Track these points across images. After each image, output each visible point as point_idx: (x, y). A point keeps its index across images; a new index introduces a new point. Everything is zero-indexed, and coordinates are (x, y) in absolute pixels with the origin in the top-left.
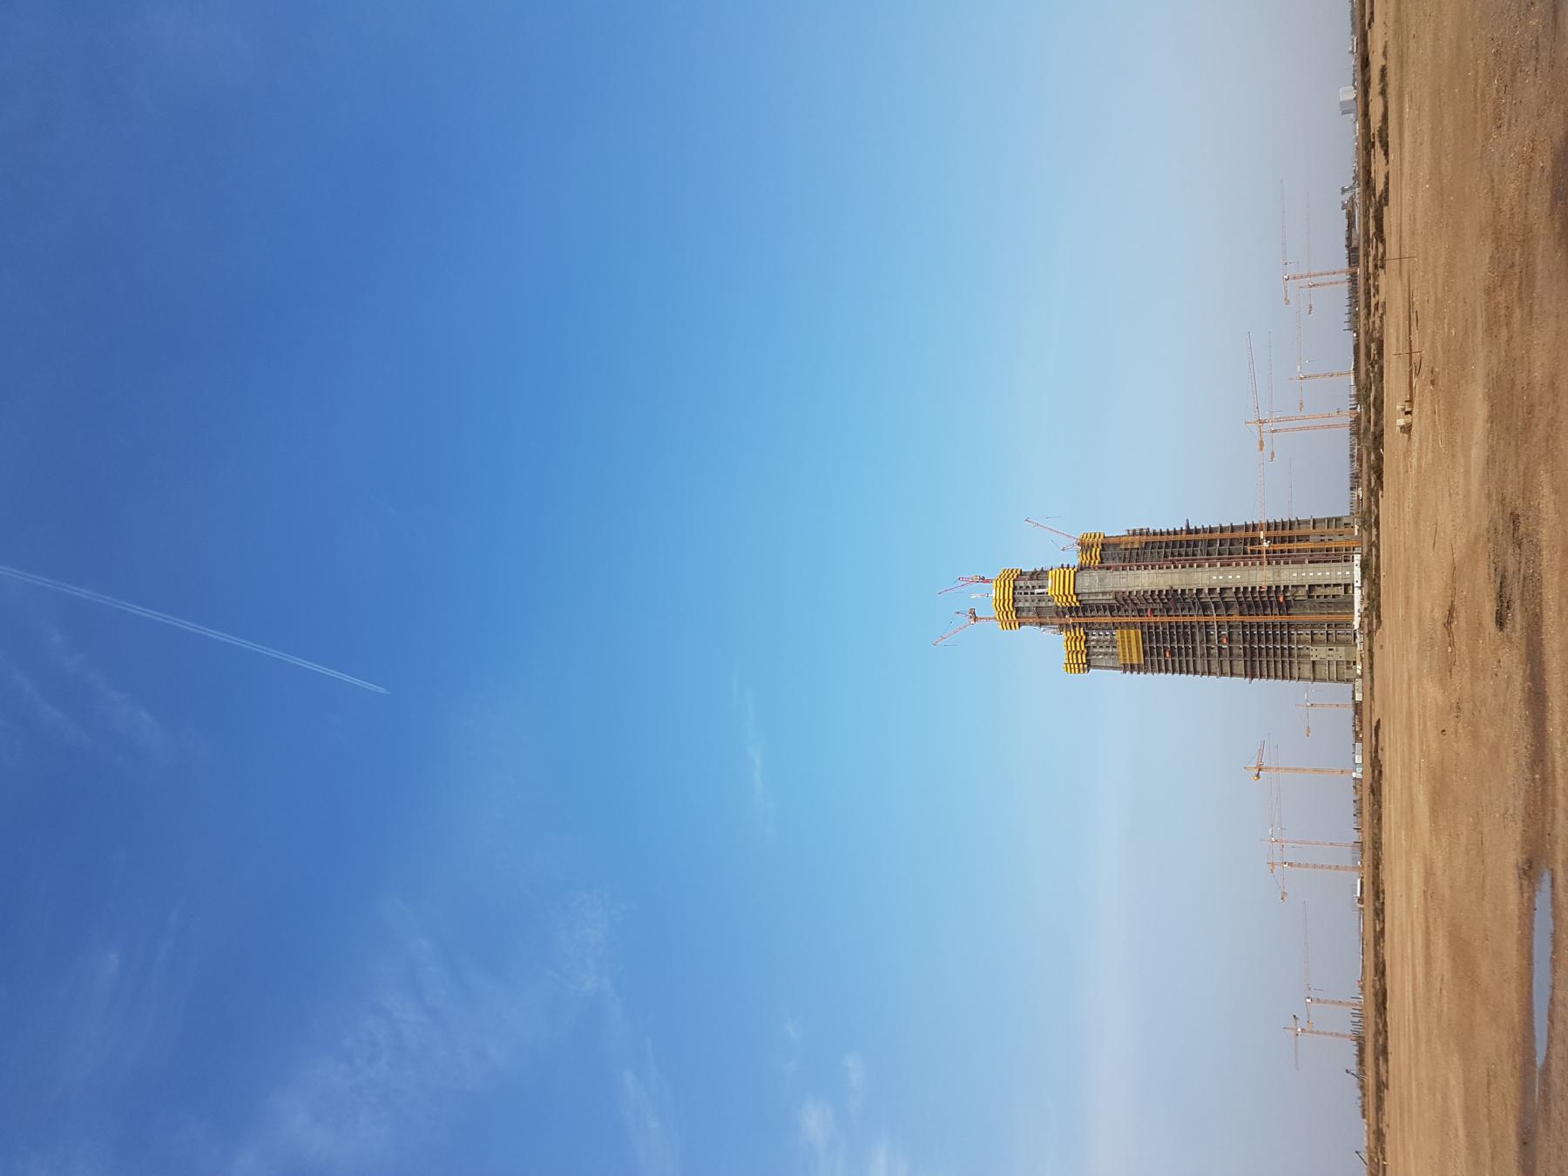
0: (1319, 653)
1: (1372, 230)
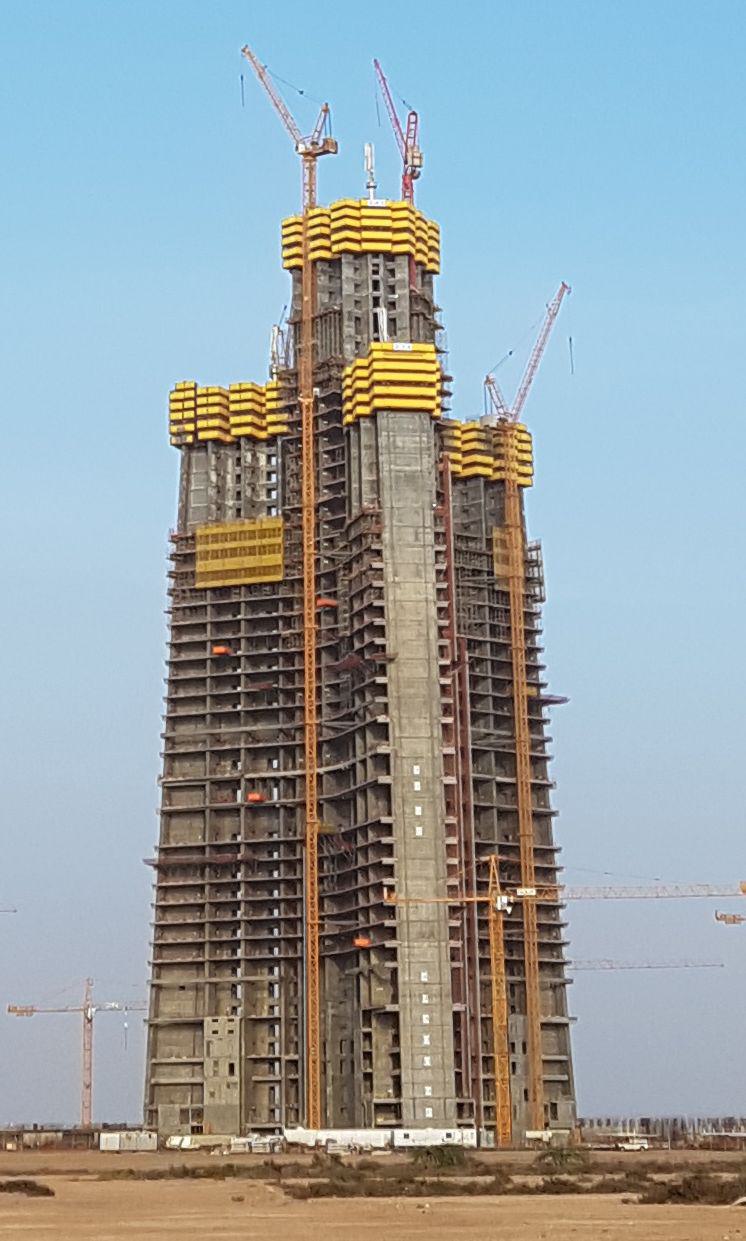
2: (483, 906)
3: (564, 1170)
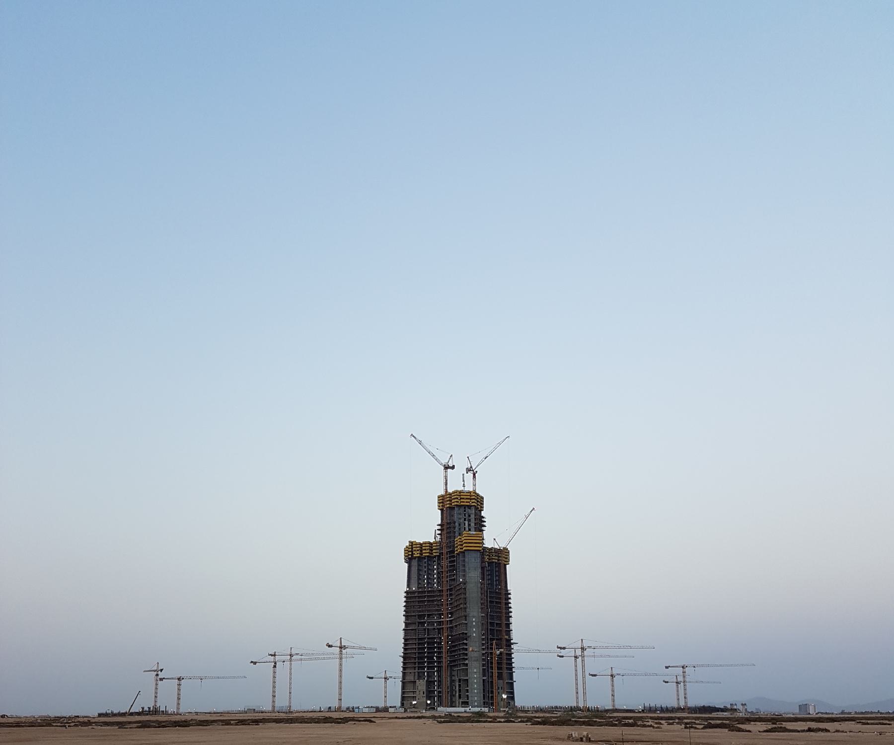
1: (712, 722)
2: (491, 653)
3: (514, 714)
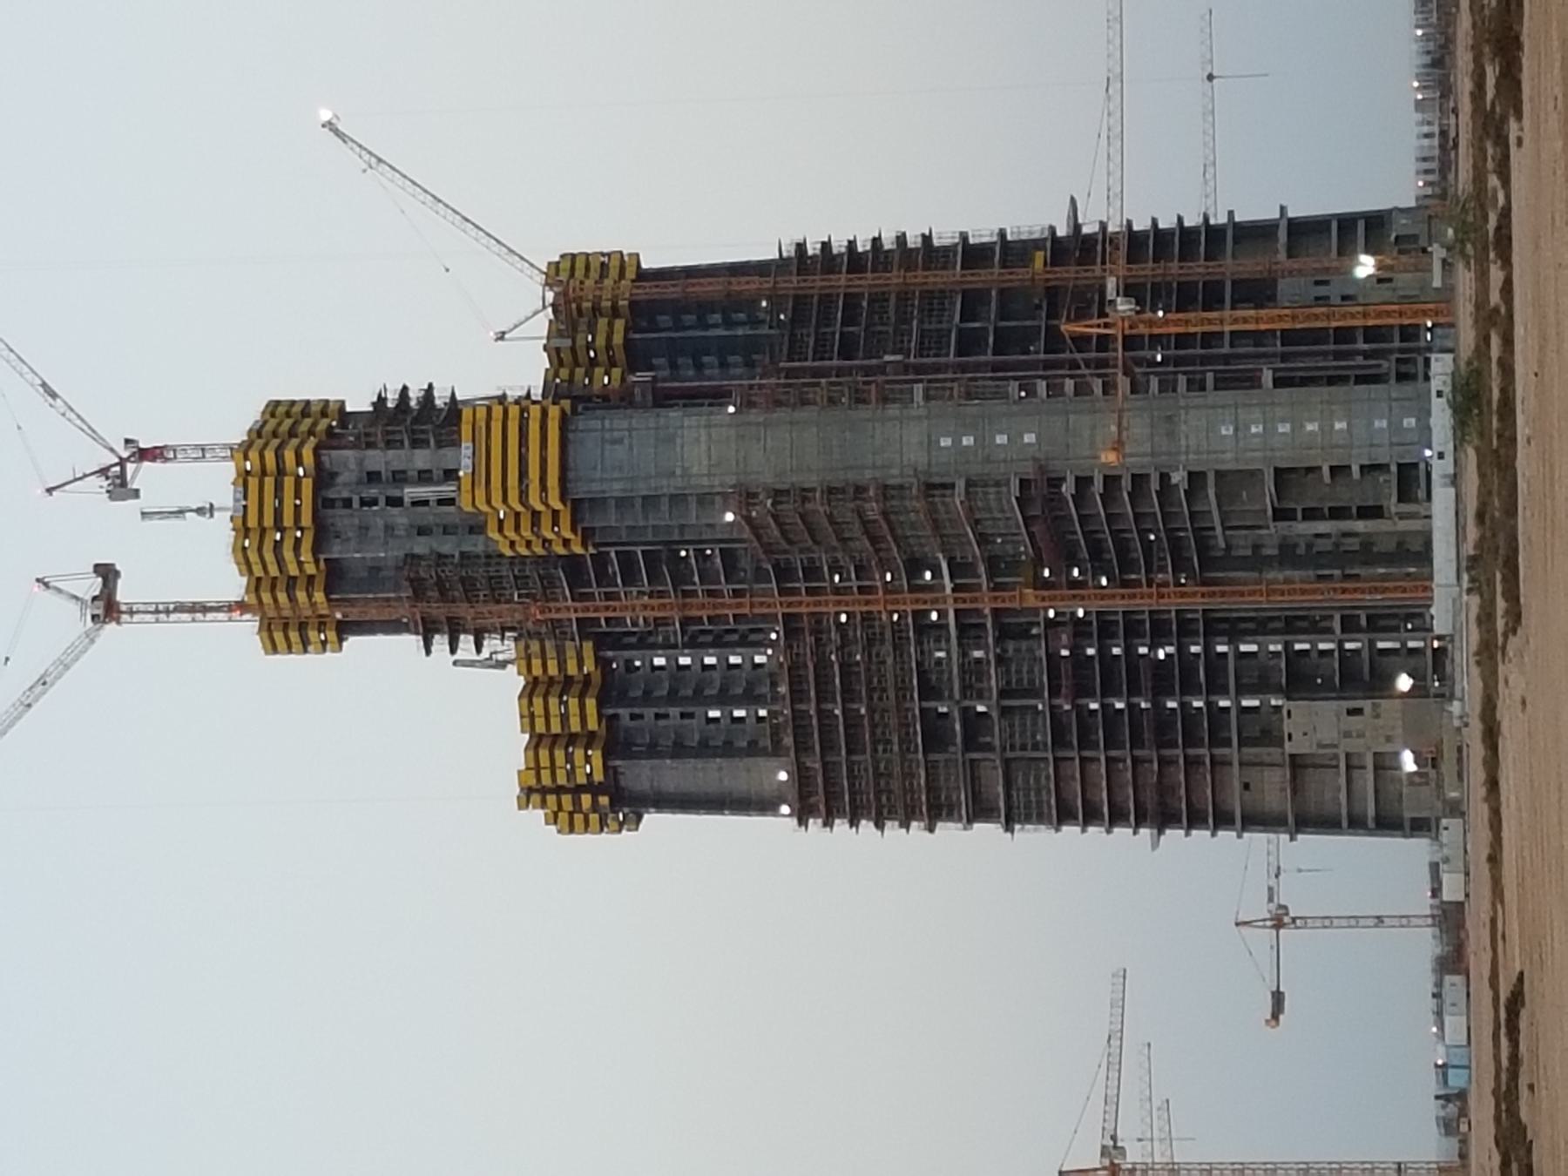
0: (1312, 724)
